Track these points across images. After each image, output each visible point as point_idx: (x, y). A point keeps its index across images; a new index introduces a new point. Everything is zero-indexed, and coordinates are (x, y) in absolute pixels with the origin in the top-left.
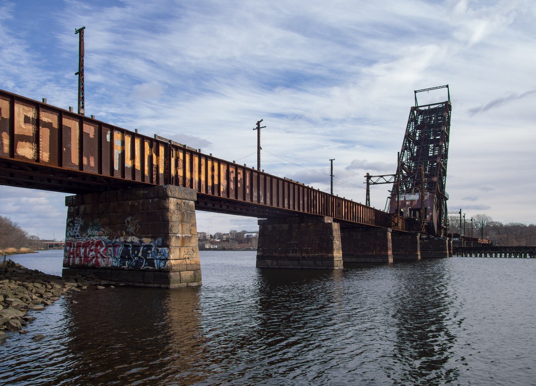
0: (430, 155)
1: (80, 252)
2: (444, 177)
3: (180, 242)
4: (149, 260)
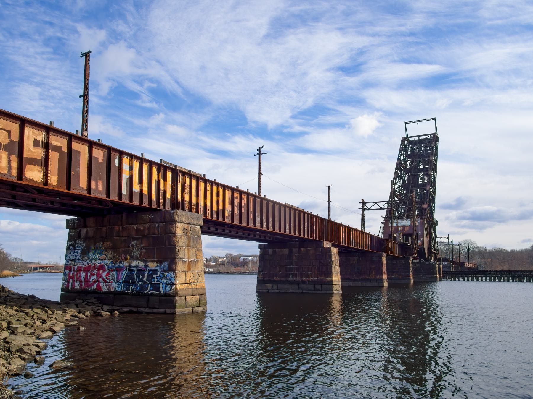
0: (420, 183)
1: (80, 276)
2: (433, 204)
3: (186, 267)
4: (155, 285)
